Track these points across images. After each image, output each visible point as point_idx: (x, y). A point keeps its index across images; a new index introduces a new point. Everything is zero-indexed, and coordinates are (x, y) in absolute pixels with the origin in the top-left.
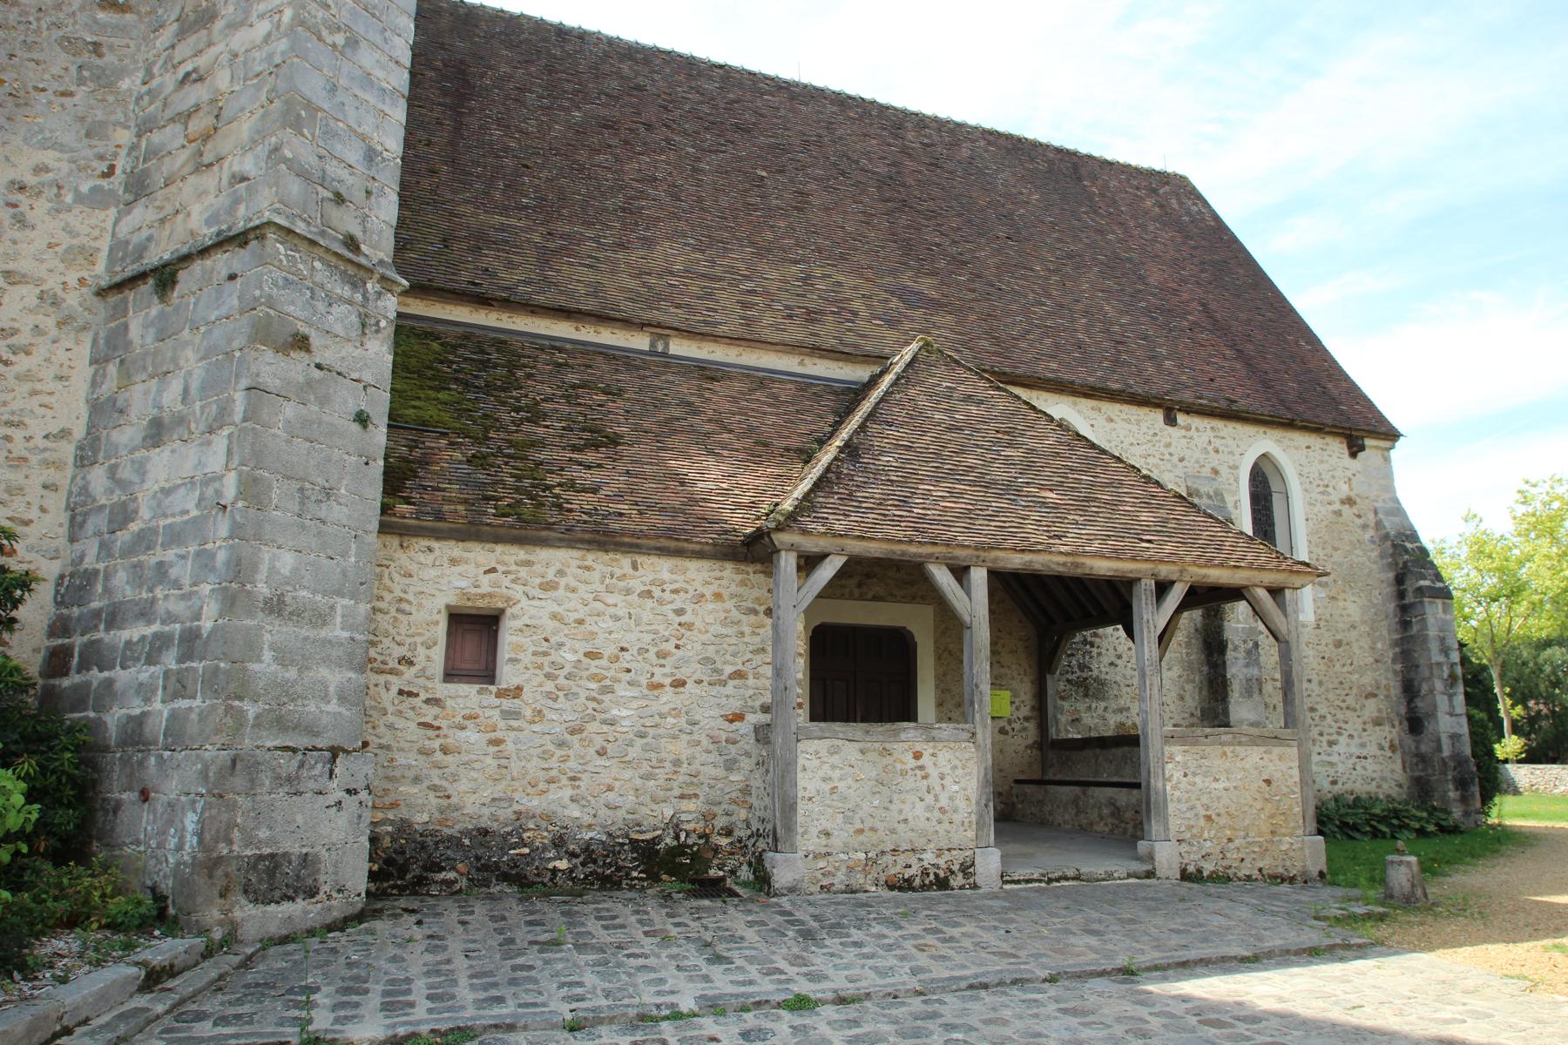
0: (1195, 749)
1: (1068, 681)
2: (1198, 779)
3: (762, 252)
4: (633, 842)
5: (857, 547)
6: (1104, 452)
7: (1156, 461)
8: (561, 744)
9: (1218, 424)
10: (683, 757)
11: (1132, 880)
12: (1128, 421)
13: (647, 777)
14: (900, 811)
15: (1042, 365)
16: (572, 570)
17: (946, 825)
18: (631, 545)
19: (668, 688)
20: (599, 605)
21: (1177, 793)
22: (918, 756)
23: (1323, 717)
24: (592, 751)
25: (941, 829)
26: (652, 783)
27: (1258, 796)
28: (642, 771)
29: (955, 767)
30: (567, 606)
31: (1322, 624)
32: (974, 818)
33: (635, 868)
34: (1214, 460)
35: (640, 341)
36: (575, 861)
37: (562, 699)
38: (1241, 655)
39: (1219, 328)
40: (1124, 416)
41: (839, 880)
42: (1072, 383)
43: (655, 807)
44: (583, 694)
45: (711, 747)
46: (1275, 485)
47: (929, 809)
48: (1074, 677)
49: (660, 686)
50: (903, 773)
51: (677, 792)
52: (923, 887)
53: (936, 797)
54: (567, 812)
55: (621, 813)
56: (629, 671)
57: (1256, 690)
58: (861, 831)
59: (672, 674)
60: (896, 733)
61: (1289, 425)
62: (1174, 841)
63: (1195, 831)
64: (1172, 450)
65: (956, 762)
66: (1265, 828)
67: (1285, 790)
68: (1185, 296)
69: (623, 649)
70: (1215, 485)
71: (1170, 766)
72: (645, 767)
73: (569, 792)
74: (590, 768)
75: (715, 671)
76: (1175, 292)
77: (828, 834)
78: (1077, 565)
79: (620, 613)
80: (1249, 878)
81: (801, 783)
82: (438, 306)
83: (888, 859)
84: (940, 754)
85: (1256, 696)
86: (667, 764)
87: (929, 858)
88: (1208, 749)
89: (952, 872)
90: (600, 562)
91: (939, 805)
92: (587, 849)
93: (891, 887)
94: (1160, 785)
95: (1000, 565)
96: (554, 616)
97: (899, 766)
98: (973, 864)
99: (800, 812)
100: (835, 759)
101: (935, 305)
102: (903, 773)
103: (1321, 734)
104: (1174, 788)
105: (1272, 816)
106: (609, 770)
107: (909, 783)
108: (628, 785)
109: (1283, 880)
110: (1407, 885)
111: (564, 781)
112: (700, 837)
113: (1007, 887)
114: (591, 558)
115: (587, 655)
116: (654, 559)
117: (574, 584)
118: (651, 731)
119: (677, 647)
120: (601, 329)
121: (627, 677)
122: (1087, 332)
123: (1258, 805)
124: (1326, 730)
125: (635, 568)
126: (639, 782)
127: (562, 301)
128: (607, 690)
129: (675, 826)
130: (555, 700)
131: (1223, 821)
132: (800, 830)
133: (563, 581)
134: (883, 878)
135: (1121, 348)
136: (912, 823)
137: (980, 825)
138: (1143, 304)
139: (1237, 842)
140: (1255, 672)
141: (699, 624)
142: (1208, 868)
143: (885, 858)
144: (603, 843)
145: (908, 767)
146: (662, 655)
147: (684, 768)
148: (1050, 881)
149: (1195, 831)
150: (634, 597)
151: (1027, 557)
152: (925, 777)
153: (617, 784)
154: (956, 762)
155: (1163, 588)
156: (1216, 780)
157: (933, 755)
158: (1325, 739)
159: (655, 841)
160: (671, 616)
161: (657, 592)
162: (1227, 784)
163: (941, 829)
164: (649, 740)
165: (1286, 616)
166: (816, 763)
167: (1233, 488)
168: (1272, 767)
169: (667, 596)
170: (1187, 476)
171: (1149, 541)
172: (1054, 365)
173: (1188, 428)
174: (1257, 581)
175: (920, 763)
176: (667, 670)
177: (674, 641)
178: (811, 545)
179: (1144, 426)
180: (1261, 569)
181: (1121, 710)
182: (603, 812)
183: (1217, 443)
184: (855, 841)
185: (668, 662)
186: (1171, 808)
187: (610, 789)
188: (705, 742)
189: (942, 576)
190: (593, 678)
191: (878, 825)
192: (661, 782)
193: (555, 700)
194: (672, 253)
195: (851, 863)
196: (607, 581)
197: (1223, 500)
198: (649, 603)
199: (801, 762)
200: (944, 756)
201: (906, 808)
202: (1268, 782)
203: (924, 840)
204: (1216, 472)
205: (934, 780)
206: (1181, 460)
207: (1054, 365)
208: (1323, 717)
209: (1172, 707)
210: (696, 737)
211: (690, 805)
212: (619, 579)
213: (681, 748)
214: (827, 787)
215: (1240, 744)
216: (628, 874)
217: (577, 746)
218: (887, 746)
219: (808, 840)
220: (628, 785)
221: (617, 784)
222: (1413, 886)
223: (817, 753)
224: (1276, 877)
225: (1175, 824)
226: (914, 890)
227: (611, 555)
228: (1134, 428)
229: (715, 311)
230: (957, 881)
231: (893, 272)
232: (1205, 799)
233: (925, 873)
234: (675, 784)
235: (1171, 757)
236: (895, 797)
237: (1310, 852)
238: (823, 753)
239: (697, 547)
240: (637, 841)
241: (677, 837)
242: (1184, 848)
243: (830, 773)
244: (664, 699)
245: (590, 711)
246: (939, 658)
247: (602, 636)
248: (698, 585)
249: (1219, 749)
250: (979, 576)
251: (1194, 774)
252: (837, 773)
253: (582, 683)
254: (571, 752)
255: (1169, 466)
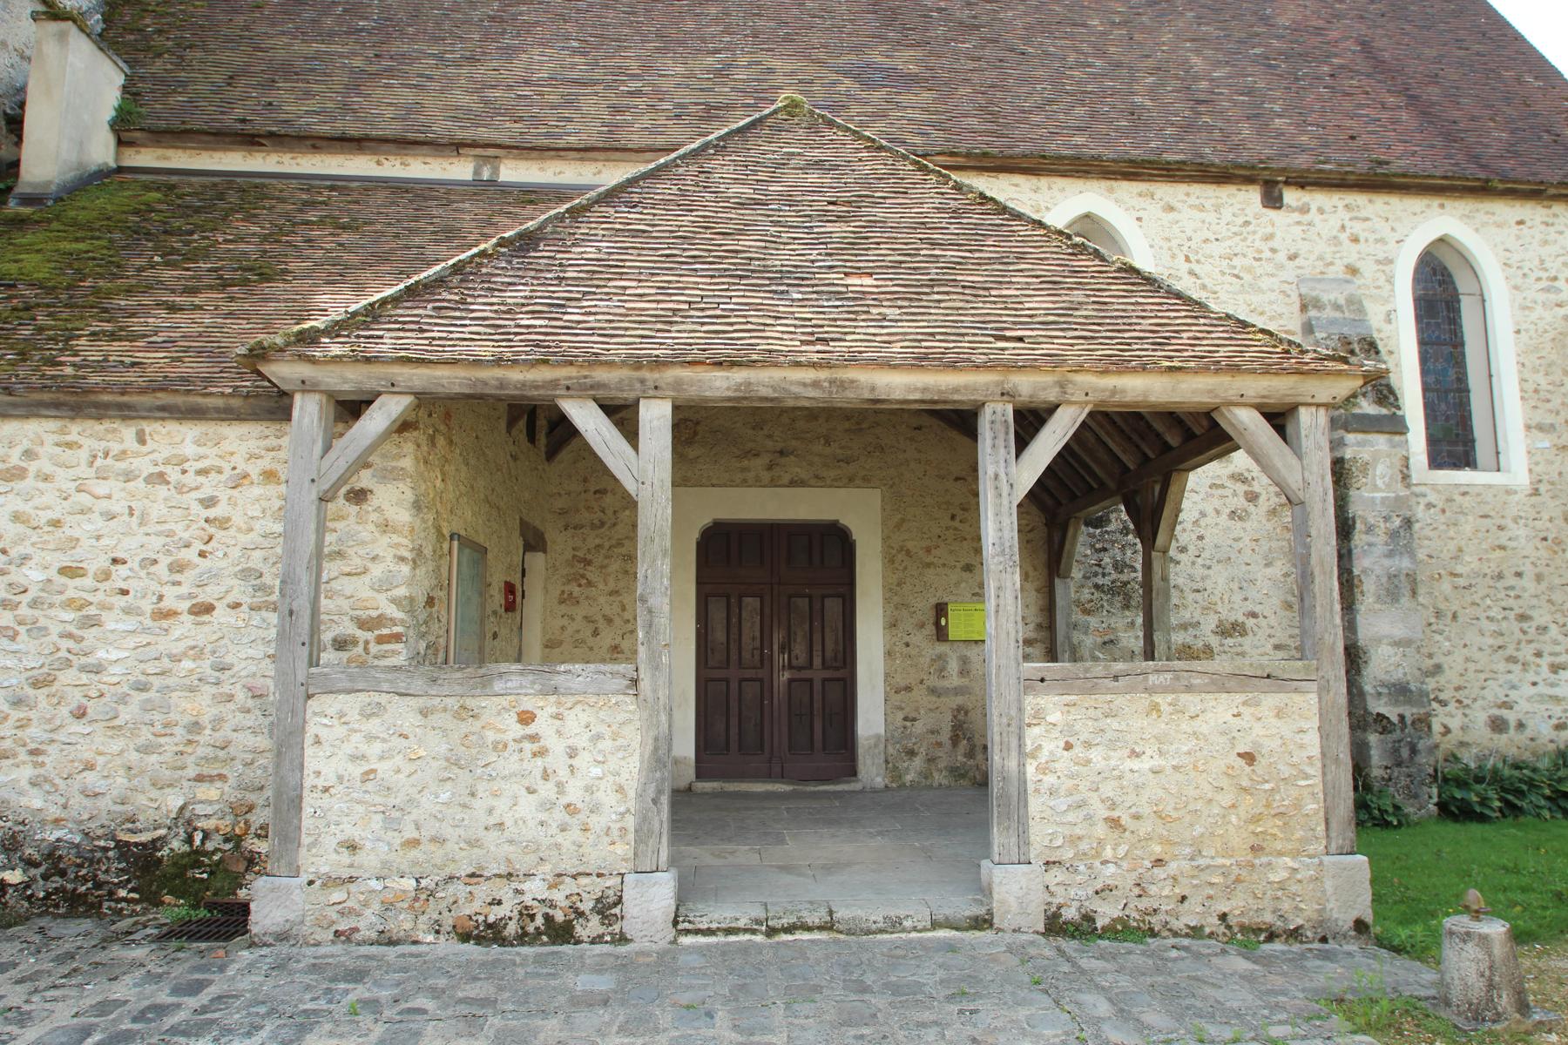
0: (1089, 701)
1: (1097, 587)
2: (1095, 755)
3: (667, 43)
4: (121, 846)
5: (419, 377)
6: (1018, 216)
7: (1248, 261)
8: (18, 703)
9: (1359, 199)
10: (205, 720)
11: (942, 934)
12: (1201, 208)
13: (145, 750)
14: (490, 811)
15: (1060, 140)
16: (49, 449)
17: (575, 834)
18: (121, 407)
19: (186, 618)
20: (84, 499)
21: (1050, 779)
22: (526, 718)
23: (1543, 629)
24: (64, 711)
25: (566, 840)
26: (154, 758)
27: (1225, 782)
28: (141, 741)
29: (598, 737)
30: (37, 501)
31: (1543, 488)
32: (630, 822)
33: (120, 885)
34: (1351, 254)
35: (460, 170)
36: (33, 872)
37: (23, 636)
38: (1380, 538)
39: (1379, 67)
40: (1192, 200)
41: (367, 924)
42: (1098, 158)
43: (154, 793)
44: (55, 630)
45: (250, 703)
46: (1463, 284)
47: (548, 806)
48: (1107, 581)
49: (171, 614)
50: (500, 747)
51: (192, 772)
52: (523, 938)
53: (560, 786)
54: (24, 801)
55: (105, 804)
56: (125, 592)
57: (1407, 592)
58: (414, 843)
59: (191, 596)
60: (485, 682)
61: (1481, 189)
62: (1038, 865)
63: (1084, 846)
64: (1274, 244)
65: (603, 729)
66: (1239, 841)
67: (1286, 772)
68: (1334, 34)
69: (115, 561)
70: (1349, 289)
71: (1036, 730)
72: (146, 735)
73: (27, 772)
74: (61, 736)
75: (257, 589)
76: (1318, 31)
77: (353, 847)
78: (842, 385)
79: (118, 507)
80: (1196, 932)
81: (311, 764)
82: (205, 155)
83: (459, 889)
84: (570, 717)
85: (1405, 601)
86: (178, 731)
87: (535, 889)
88: (1120, 700)
89: (580, 914)
90: (87, 435)
91: (564, 800)
92: (50, 855)
93: (465, 937)
94: (1012, 764)
95: (692, 392)
96: (17, 517)
97: (491, 736)
98: (619, 901)
99: (307, 811)
100: (374, 725)
101: (910, 81)
102: (500, 747)
103: (1539, 654)
104: (1043, 770)
105: (1256, 819)
106: (91, 741)
107: (509, 763)
108: (119, 761)
109: (1271, 937)
110: (1478, 987)
111: (23, 756)
112: (227, 840)
113: (686, 940)
114: (77, 430)
115: (64, 571)
116: (172, 427)
117: (48, 468)
118: (157, 682)
119: (202, 554)
120: (410, 160)
121: (122, 601)
122: (1152, 92)
123: (1226, 799)
124: (1547, 649)
125: (142, 441)
126: (134, 756)
127: (354, 130)
128: (92, 622)
129: (185, 819)
130: (13, 639)
131: (1144, 828)
132: (306, 840)
133: (33, 467)
134: (448, 922)
135: (1202, 108)
136: (511, 831)
137: (642, 835)
138: (1257, 51)
139: (1173, 867)
140: (1405, 563)
141: (238, 520)
142: (1106, 913)
143: (451, 888)
144: (77, 846)
145: (509, 736)
146: (178, 567)
147: (206, 736)
148: (772, 931)
149: (1084, 846)
150: (139, 484)
151: (739, 375)
152: (541, 753)
153: (101, 760)
154: (603, 729)
155: (1029, 421)
156: (1135, 754)
157: (558, 717)
158: (1545, 661)
159: (155, 844)
160: (196, 508)
161: (173, 474)
162: (1158, 762)
163: (566, 840)
164: (152, 694)
165: (1300, 458)
166: (341, 731)
167: (1385, 293)
168: (1258, 730)
169: (191, 479)
170: (1301, 280)
171: (1020, 339)
172: (1079, 140)
173: (1304, 210)
174: (1232, 395)
175: (531, 729)
176: (184, 590)
177: (198, 546)
178: (349, 379)
179: (1227, 214)
180: (1234, 369)
181: (1184, 627)
182: (77, 801)
183: (1357, 228)
184: (403, 860)
185: (188, 578)
186: (1035, 805)
187: (89, 767)
188: (241, 696)
189: (587, 419)
190: (69, 604)
191: (448, 831)
192: (168, 757)
193: (13, 639)
194: (540, 61)
195: (390, 896)
196: (99, 462)
197: (1361, 310)
198: (162, 491)
199: (311, 730)
200: (578, 719)
201: (502, 805)
202: (1249, 758)
203: (533, 858)
204: (1353, 271)
205: (557, 759)
206: (1293, 257)
207: (1079, 140)
208: (1543, 629)
209: (1273, 620)
210: (226, 688)
211: (210, 792)
212: (118, 458)
213: (202, 705)
214: (357, 770)
215: (1189, 689)
216: (111, 893)
217: (43, 704)
218: (470, 702)
219: (320, 857)
220: (119, 761)
221: (101, 760)
222: (1491, 986)
223: (342, 715)
224: (1257, 931)
225: (1040, 834)
226: (504, 942)
227: (107, 424)
228: (1211, 217)
229: (570, 120)
230: (590, 927)
231: (857, 49)
232: (1108, 790)
233: (526, 914)
234: (190, 760)
235: (1039, 715)
236: (481, 788)
237: (1340, 883)
238: (353, 716)
239: (220, 402)
240: (127, 844)
241: (189, 840)
242: (1056, 876)
243: (364, 748)
244: (177, 633)
245: (63, 654)
246: (890, 561)
247: (86, 543)
248: (239, 461)
249: (1143, 700)
250: (656, 417)
251: (1088, 745)
252: (377, 747)
253: (52, 612)
254: (33, 714)
255: (1269, 268)
